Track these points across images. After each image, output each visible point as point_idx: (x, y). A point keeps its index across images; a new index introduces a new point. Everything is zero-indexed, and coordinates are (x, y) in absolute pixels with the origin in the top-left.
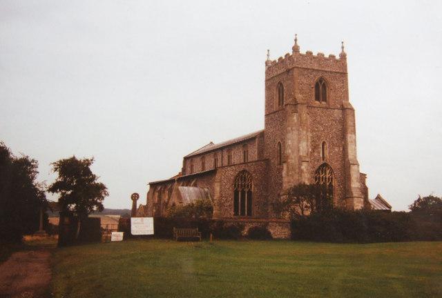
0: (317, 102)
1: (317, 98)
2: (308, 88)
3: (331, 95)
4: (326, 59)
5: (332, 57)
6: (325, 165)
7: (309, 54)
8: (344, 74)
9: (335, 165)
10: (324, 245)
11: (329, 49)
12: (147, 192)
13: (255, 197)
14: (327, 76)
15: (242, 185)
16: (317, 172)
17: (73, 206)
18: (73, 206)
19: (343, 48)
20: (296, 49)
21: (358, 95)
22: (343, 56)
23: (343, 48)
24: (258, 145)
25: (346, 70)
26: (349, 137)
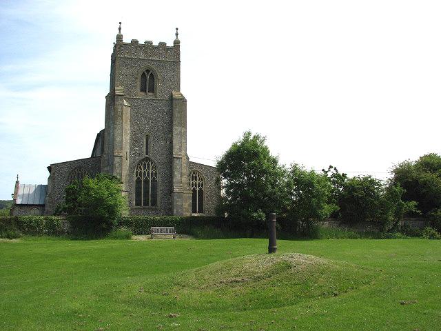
0: (143, 93)
1: (143, 90)
2: (146, 78)
3: (159, 86)
4: (156, 47)
5: (162, 45)
6: (147, 159)
7: (135, 42)
8: (176, 63)
9: (158, 157)
10: (101, 241)
11: (160, 35)
12: (427, 154)
13: (205, 195)
14: (153, 66)
15: (145, 173)
16: (138, 167)
17: (226, 214)
18: (226, 214)
19: (177, 34)
20: (119, 38)
21: (189, 86)
22: (177, 43)
23: (177, 34)
24: (132, 125)
25: (179, 58)
26: (177, 129)
